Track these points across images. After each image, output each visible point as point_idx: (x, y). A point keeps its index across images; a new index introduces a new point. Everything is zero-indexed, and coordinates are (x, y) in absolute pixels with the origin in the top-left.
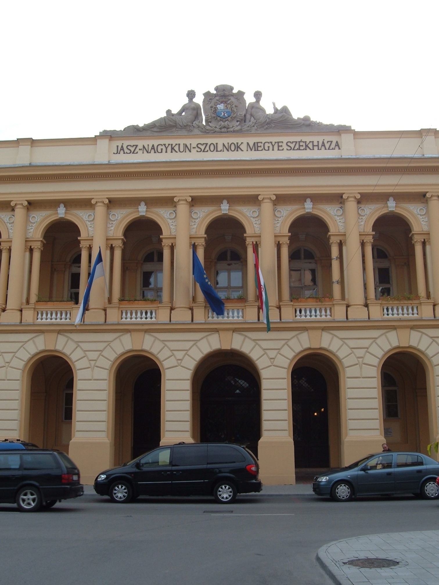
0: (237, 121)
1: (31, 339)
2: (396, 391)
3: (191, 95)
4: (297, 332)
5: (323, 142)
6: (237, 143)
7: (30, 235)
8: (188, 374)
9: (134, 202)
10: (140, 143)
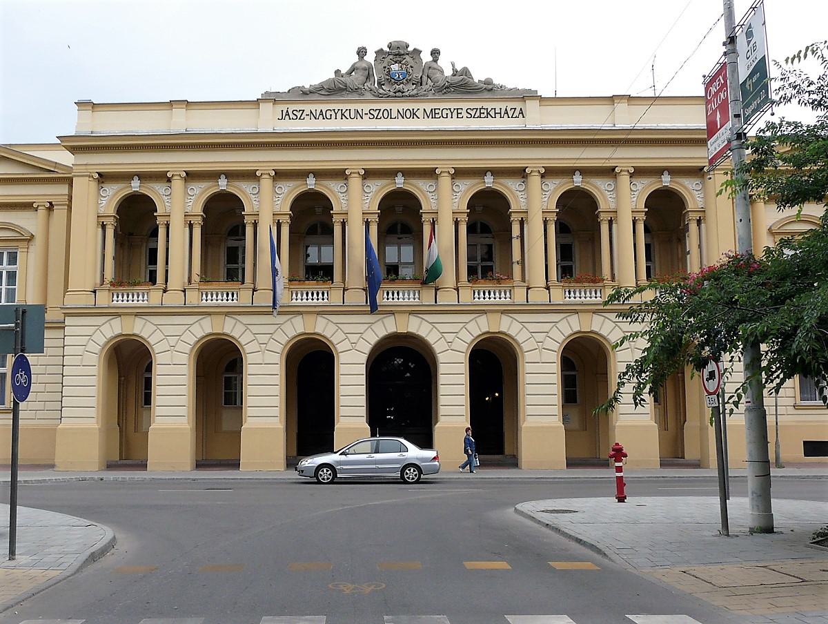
0: (413, 84)
1: (564, 318)
2: (575, 376)
3: (362, 52)
4: (291, 316)
5: (506, 110)
6: (413, 109)
7: (189, 209)
8: (363, 358)
9: (127, 177)
10: (308, 108)
